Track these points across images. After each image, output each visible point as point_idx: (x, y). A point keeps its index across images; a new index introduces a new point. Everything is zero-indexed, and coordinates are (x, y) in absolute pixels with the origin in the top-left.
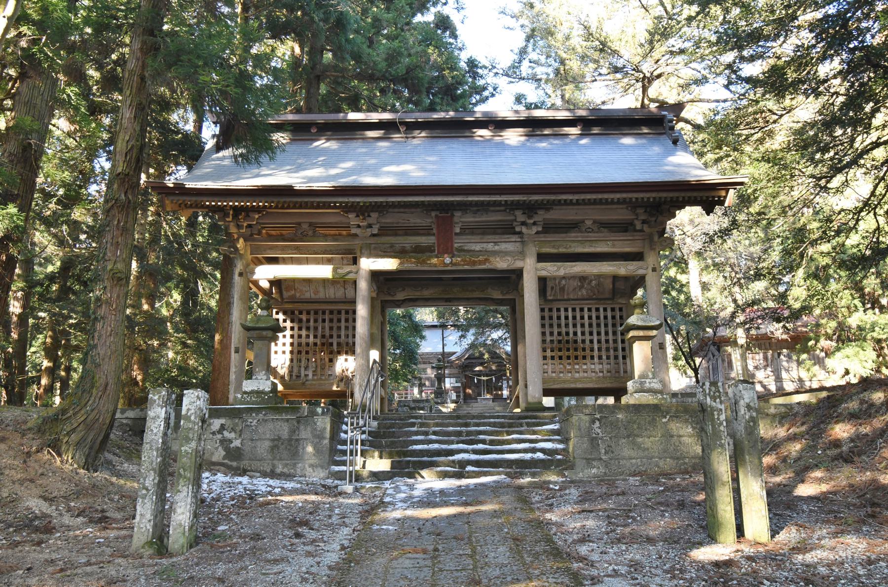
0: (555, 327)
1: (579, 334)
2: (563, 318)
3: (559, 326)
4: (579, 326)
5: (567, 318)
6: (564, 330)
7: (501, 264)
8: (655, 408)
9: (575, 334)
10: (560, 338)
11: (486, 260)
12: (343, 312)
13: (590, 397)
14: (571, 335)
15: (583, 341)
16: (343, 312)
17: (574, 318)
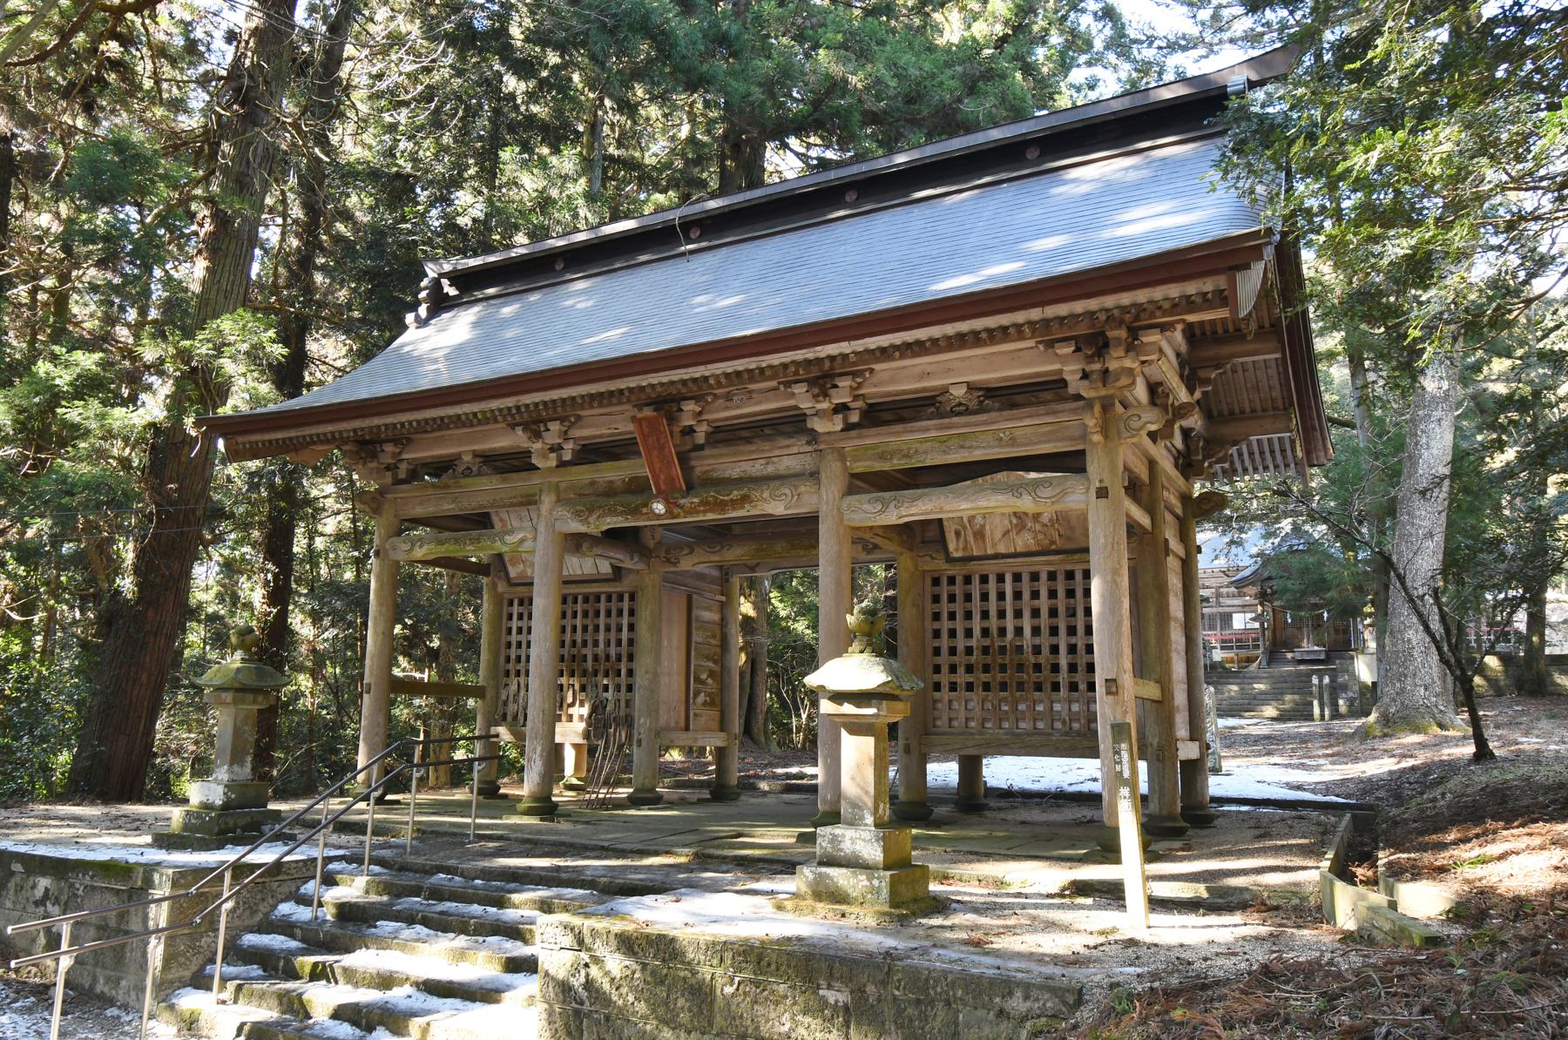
0: (977, 617)
1: (1027, 631)
2: (993, 596)
3: (985, 615)
4: (1027, 614)
5: (1001, 596)
6: (993, 623)
7: (776, 506)
8: (1422, 833)
9: (1019, 631)
10: (987, 642)
11: (745, 499)
12: (603, 598)
13: (985, 772)
14: (1010, 635)
15: (1037, 650)
16: (603, 598)
17: (1018, 595)
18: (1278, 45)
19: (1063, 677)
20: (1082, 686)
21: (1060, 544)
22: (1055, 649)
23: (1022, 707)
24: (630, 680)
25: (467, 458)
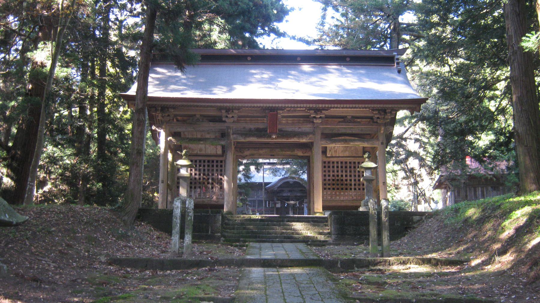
18: (465, 264)
19: (353, 187)
20: (361, 189)
21: (354, 155)
22: (351, 180)
23: (342, 193)
24: (340, 189)
25: (198, 116)
